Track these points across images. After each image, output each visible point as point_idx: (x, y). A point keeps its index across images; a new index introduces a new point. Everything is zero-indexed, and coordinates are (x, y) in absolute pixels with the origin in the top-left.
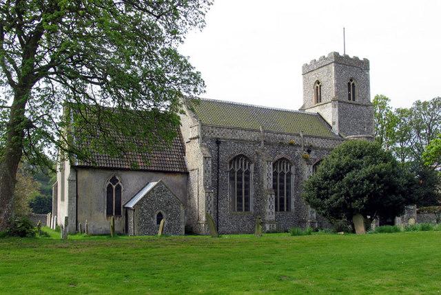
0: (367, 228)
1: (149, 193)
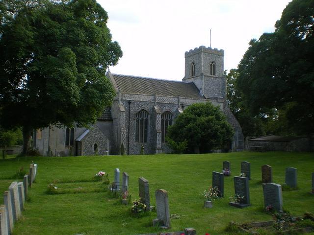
1: (85, 136)
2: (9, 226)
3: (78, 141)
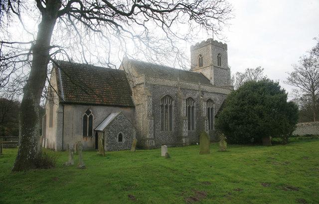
0: (54, 146)
1: (109, 125)
2: (45, 140)
3: (99, 131)
